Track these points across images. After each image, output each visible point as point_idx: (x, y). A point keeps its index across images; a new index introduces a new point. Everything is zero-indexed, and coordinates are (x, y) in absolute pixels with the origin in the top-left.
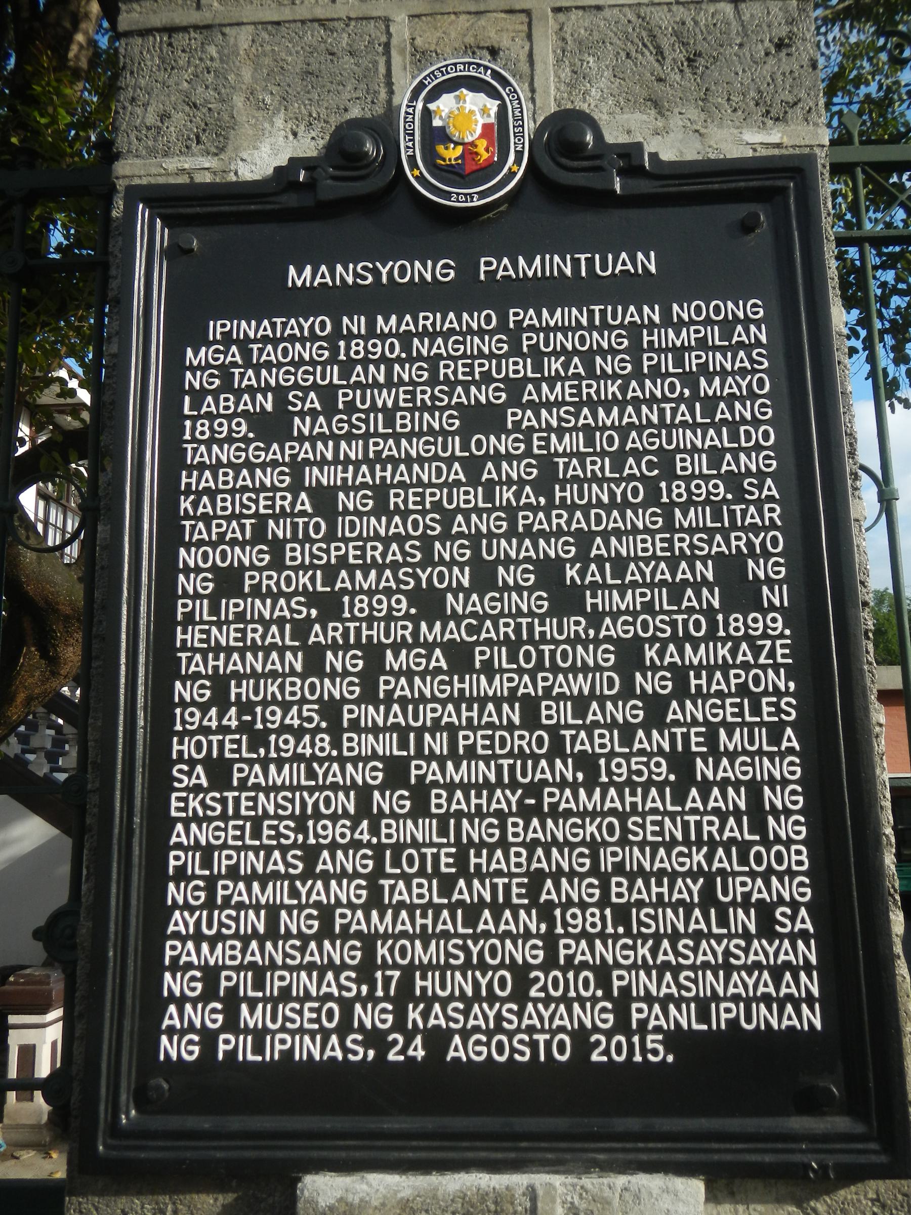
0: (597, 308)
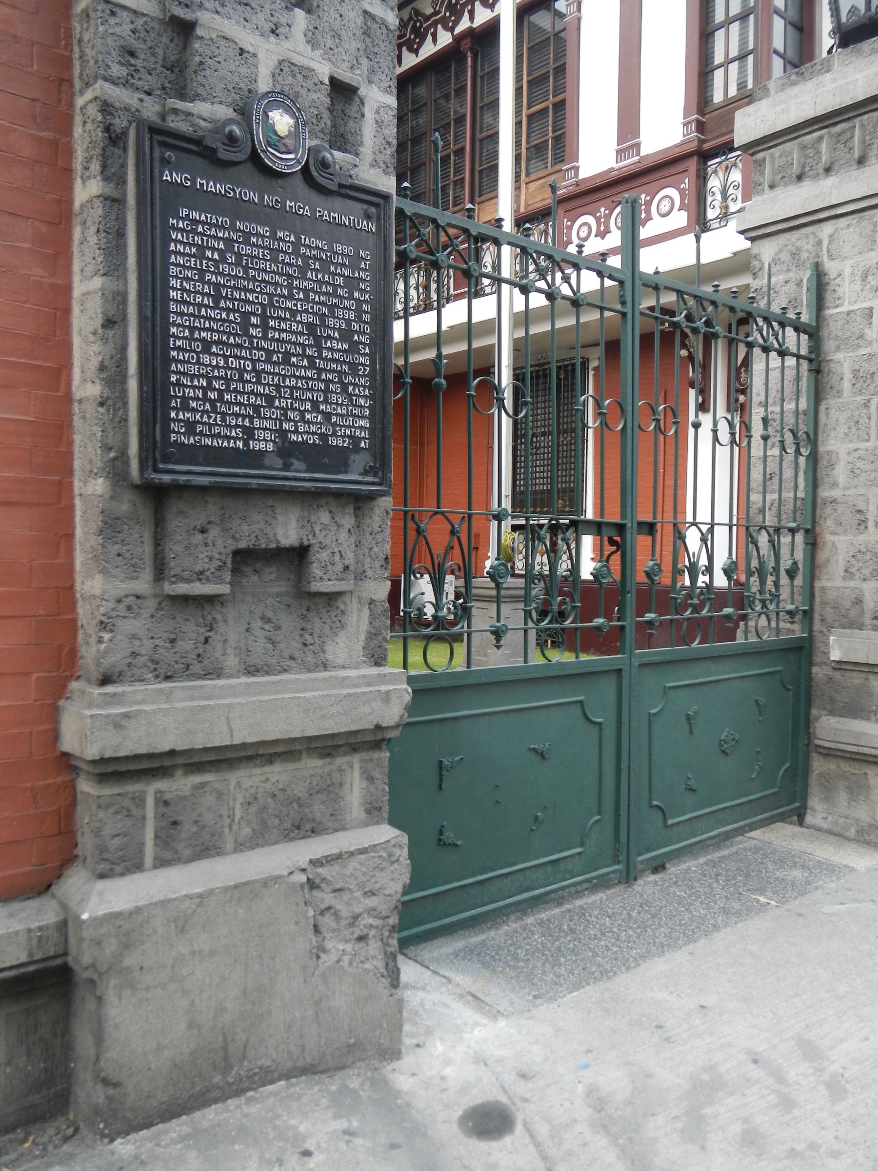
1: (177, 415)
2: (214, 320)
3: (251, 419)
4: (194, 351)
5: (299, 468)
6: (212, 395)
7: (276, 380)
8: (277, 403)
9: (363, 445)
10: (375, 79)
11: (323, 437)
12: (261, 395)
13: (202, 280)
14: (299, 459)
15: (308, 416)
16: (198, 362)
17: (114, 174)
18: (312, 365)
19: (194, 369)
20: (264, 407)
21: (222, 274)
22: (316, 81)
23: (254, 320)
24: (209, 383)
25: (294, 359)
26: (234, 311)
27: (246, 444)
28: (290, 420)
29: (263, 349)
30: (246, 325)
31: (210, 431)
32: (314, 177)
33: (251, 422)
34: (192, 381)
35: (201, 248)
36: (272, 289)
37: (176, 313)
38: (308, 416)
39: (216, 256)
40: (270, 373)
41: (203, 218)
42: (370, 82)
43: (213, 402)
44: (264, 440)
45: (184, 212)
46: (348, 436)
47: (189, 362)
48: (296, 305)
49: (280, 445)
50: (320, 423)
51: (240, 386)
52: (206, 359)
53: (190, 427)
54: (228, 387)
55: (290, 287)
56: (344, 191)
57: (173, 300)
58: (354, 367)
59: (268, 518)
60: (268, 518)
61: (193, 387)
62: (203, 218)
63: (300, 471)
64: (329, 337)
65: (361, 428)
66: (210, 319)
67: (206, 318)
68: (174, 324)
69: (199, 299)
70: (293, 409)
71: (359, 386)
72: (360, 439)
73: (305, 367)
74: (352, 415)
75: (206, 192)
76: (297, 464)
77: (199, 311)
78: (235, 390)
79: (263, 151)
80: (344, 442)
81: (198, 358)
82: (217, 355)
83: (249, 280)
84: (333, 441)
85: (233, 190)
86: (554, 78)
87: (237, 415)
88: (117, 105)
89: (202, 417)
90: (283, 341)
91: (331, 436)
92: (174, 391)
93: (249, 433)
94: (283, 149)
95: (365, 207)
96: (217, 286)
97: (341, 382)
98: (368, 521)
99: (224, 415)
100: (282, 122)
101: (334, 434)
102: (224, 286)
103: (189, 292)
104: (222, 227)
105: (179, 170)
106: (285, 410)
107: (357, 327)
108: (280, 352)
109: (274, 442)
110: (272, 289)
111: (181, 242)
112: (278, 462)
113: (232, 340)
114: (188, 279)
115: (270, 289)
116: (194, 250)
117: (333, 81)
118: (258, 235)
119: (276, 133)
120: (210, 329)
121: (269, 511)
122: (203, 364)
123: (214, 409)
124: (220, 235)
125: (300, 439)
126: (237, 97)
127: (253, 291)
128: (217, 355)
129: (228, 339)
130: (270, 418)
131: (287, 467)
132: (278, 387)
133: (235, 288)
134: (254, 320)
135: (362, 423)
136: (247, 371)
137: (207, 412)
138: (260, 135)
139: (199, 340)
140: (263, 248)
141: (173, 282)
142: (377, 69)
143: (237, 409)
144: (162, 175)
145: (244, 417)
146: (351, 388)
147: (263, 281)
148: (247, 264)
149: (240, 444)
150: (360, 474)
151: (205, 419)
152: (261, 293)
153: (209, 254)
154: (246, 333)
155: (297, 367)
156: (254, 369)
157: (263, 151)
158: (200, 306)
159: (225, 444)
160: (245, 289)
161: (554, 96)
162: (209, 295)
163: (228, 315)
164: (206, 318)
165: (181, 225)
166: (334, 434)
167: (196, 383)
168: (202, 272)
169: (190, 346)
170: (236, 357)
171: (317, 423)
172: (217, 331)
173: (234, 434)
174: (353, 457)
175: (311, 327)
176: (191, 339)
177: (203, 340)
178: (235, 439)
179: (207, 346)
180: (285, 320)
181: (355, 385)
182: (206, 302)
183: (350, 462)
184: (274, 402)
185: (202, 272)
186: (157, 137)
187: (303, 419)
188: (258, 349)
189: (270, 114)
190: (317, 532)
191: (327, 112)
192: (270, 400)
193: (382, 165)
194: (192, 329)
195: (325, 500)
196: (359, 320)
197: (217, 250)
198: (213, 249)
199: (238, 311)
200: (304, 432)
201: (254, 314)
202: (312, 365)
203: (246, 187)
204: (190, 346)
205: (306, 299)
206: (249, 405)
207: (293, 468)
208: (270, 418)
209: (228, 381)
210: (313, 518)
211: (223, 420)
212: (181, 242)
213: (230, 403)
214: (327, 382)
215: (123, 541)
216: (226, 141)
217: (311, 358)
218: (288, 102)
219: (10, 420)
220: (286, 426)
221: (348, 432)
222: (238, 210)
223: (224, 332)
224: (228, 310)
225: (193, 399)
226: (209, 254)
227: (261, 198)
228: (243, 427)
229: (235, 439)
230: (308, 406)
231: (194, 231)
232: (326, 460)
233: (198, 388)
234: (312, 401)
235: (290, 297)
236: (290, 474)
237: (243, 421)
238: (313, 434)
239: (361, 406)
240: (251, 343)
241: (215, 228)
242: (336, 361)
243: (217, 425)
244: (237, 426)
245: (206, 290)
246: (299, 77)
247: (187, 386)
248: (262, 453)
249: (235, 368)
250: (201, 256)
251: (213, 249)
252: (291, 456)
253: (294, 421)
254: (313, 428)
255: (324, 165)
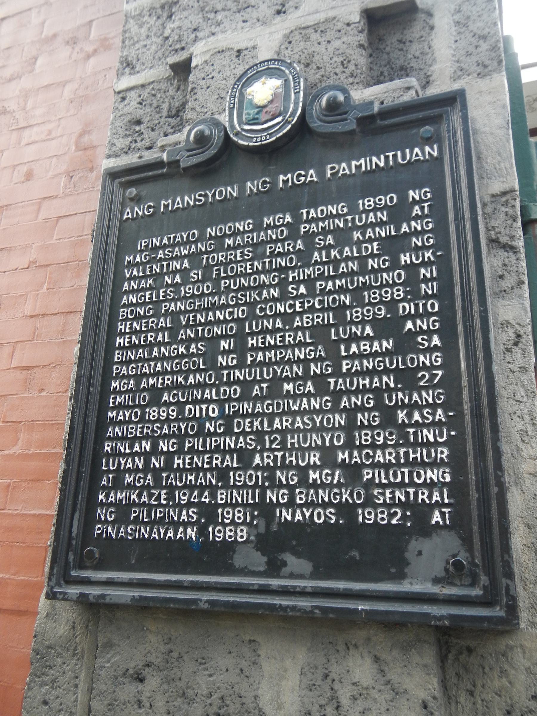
0: (390, 154)
1: (107, 496)
5: (296, 571)
6: (155, 462)
7: (256, 424)
8: (257, 460)
9: (436, 517)
11: (346, 510)
12: (231, 451)
14: (297, 554)
15: (313, 475)
18: (321, 388)
19: (136, 430)
20: (235, 469)
24: (155, 446)
25: (288, 387)
26: (196, 340)
27: (202, 531)
28: (281, 486)
31: (149, 515)
33: (213, 495)
35: (158, 277)
36: (255, 295)
38: (313, 475)
40: (248, 415)
43: (156, 472)
44: (233, 522)
46: (401, 505)
47: (130, 422)
48: (292, 306)
49: (262, 529)
50: (339, 485)
51: (198, 443)
52: (153, 413)
53: (123, 512)
54: (181, 445)
58: (408, 378)
59: (244, 664)
60: (244, 664)
61: (133, 455)
63: (301, 577)
64: (355, 339)
65: (431, 485)
70: (285, 467)
71: (420, 408)
72: (431, 507)
73: (309, 395)
74: (407, 463)
76: (293, 563)
79: (237, 134)
84: (366, 516)
87: (191, 487)
89: (139, 496)
91: (363, 506)
93: (209, 514)
97: (379, 406)
99: (171, 489)
101: (369, 502)
106: (270, 470)
107: (410, 308)
108: (264, 381)
109: (250, 525)
110: (255, 295)
112: (259, 561)
113: (191, 380)
115: (251, 296)
116: (150, 282)
121: (246, 650)
122: (149, 421)
123: (158, 484)
125: (299, 517)
130: (245, 486)
131: (274, 568)
132: (260, 435)
135: (431, 475)
136: (210, 419)
137: (148, 487)
143: (191, 478)
146: (401, 415)
148: (218, 275)
149: (192, 533)
150: (436, 581)
151: (144, 499)
153: (168, 280)
155: (295, 397)
156: (222, 415)
157: (237, 134)
159: (170, 534)
166: (369, 502)
171: (331, 486)
173: (184, 517)
174: (414, 545)
175: (319, 333)
181: (412, 407)
182: (160, 338)
183: (410, 555)
184: (253, 458)
187: (303, 482)
188: (229, 383)
190: (345, 701)
192: (245, 457)
195: (362, 634)
196: (414, 295)
199: (203, 339)
200: (307, 505)
202: (321, 388)
205: (311, 293)
206: (211, 470)
207: (285, 571)
208: (245, 486)
210: (335, 670)
211: (170, 496)
213: (182, 470)
214: (351, 413)
215: (53, 681)
217: (320, 380)
219: (34, 515)
221: (400, 495)
223: (180, 372)
224: (190, 340)
225: (129, 471)
226: (168, 280)
228: (200, 504)
230: (315, 458)
232: (355, 554)
234: (321, 448)
236: (275, 583)
237: (200, 495)
238: (325, 505)
239: (428, 444)
240: (219, 377)
242: (370, 373)
243: (160, 505)
244: (190, 504)
246: (315, 37)
247: (125, 455)
248: (229, 547)
249: (194, 418)
252: (283, 550)
253: (288, 486)
254: (324, 495)
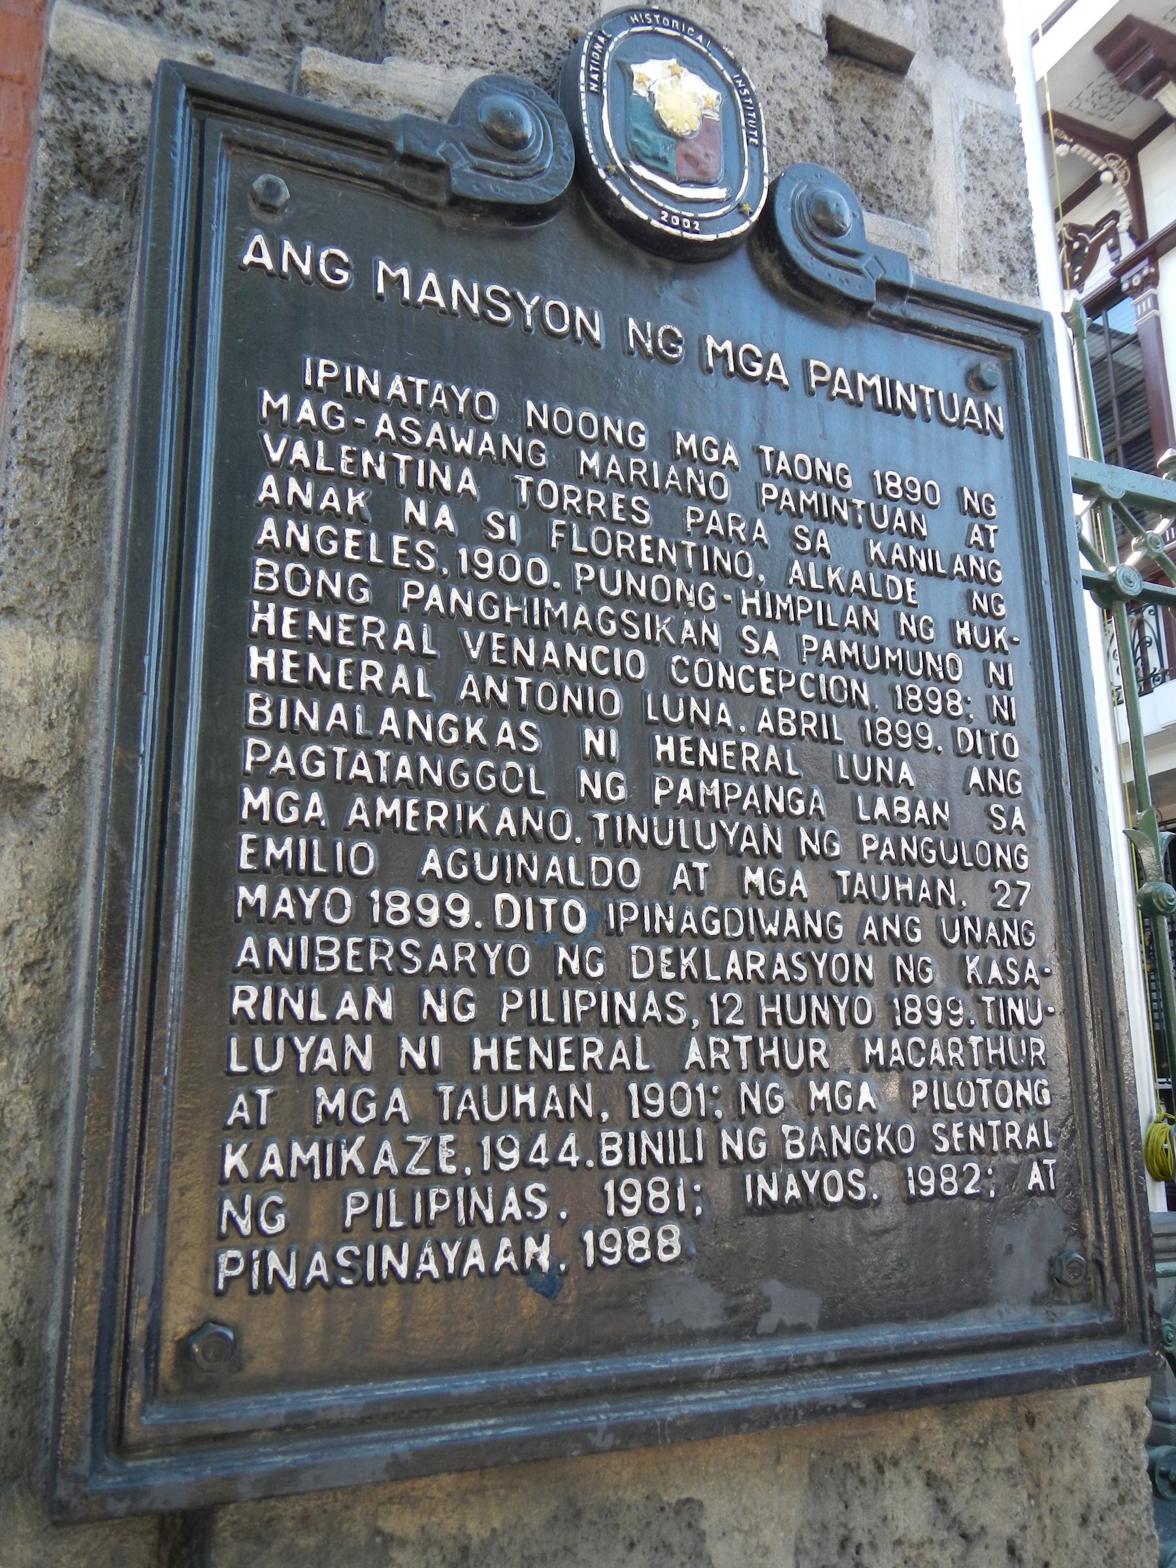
1: (255, 1157)
2: (435, 749)
3: (589, 1128)
4: (348, 878)
8: (694, 1054)
9: (1036, 1178)
10: (953, 45)
13: (386, 606)
16: (362, 922)
17: (81, 274)
20: (643, 1077)
21: (467, 582)
22: (783, 22)
23: (593, 740)
26: (516, 711)
29: (632, 844)
30: (563, 755)
32: (792, 264)
33: (590, 1146)
34: (330, 1003)
37: (273, 733)
39: (445, 517)
41: (397, 387)
42: (941, 52)
45: (323, 370)
47: (320, 923)
48: (754, 677)
52: (398, 905)
55: (729, 614)
56: (896, 309)
57: (263, 682)
62: (397, 387)
66: (413, 745)
67: (397, 745)
68: (261, 776)
69: (373, 674)
70: (761, 1070)
75: (412, 304)
77: (374, 720)
78: (524, 1021)
80: (964, 1176)
81: (363, 904)
82: (444, 884)
83: (575, 599)
85: (513, 301)
86: (1120, 409)
87: (526, 1125)
88: (116, 72)
90: (715, 811)
92: (247, 1055)
93: (579, 1195)
94: (688, 172)
95: (969, 358)
96: (448, 623)
98: (1067, 1471)
100: (679, 95)
102: (477, 622)
103: (329, 651)
104: (472, 420)
105: (304, 231)
111: (302, 473)
113: (506, 821)
114: (327, 604)
117: (832, 26)
118: (605, 444)
119: (658, 124)
120: (419, 787)
124: (464, 445)
126: (530, 51)
127: (590, 635)
128: (444, 884)
129: (491, 817)
133: (521, 628)
134: (593, 740)
138: (604, 129)
139: (370, 832)
140: (626, 486)
141: (263, 617)
142: (956, 23)
144: (236, 245)
145: (559, 1126)
147: (629, 597)
148: (566, 541)
152: (620, 639)
154: (565, 792)
156: (600, 928)
157: (618, 174)
158: (375, 700)
160: (560, 631)
161: (1122, 434)
162: (413, 658)
163: (490, 730)
164: (397, 745)
165: (306, 412)
167: (348, 1008)
168: (386, 578)
169: (329, 857)
170: (521, 884)
172: (447, 791)
176: (335, 827)
177: (387, 832)
178: (521, 1229)
179: (399, 849)
180: (714, 731)
185: (386, 578)
186: (217, 127)
188: (615, 847)
189: (635, 68)
191: (821, 104)
193: (994, 264)
194: (338, 792)
197: (450, 497)
198: (435, 496)
199: (534, 711)
201: (597, 719)
203: (555, 293)
204: (329, 857)
207: (767, 1323)
209: (487, 983)
211: (467, 1150)
212: (302, 473)
213: (496, 1077)
216: (485, 144)
218: (698, 42)
220: (732, 1143)
222: (523, 363)
224: (492, 710)
227: (616, 329)
229: (521, 1229)
231: (362, 437)
233: (359, 1026)
235: (737, 650)
237: (555, 1147)
241: (446, 436)
245: (404, 639)
250: (383, 514)
251: (435, 496)
255: (825, 226)
